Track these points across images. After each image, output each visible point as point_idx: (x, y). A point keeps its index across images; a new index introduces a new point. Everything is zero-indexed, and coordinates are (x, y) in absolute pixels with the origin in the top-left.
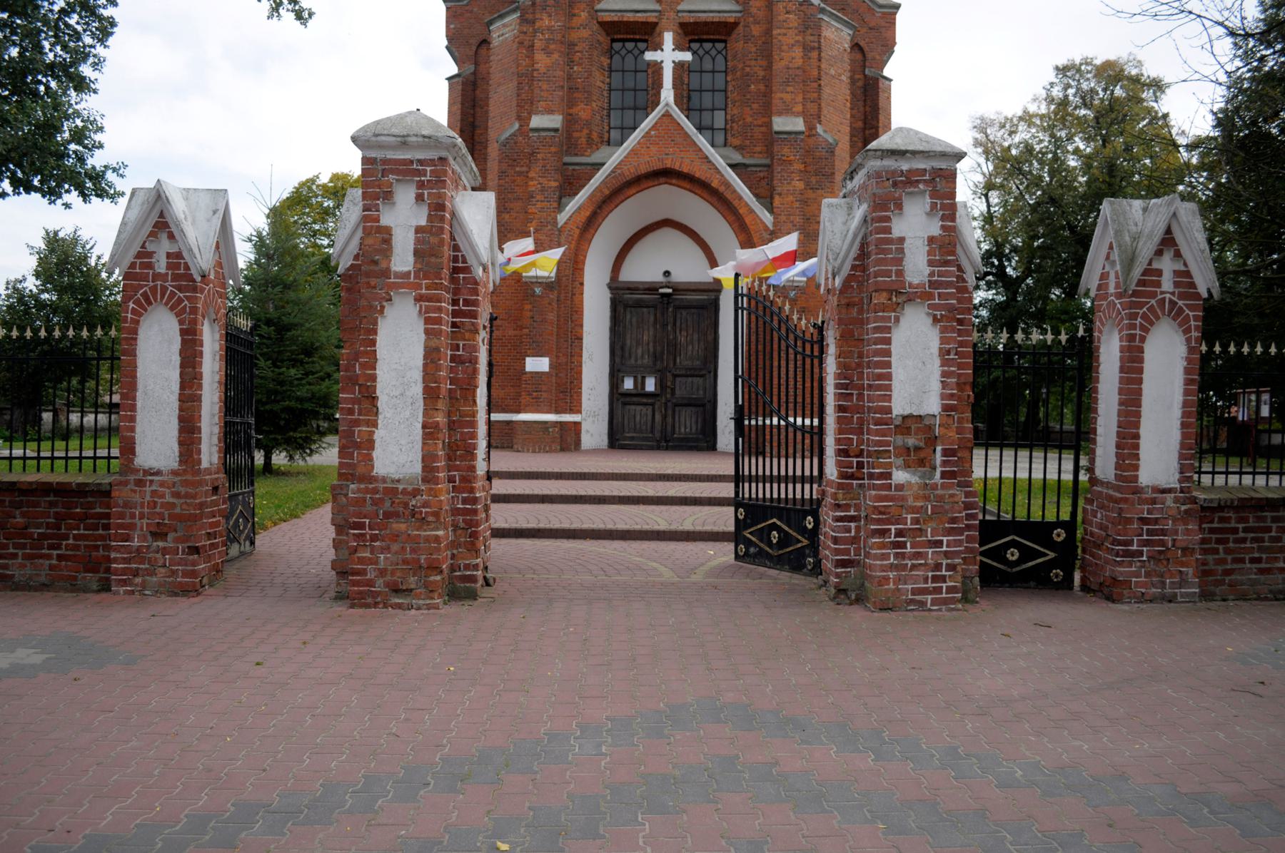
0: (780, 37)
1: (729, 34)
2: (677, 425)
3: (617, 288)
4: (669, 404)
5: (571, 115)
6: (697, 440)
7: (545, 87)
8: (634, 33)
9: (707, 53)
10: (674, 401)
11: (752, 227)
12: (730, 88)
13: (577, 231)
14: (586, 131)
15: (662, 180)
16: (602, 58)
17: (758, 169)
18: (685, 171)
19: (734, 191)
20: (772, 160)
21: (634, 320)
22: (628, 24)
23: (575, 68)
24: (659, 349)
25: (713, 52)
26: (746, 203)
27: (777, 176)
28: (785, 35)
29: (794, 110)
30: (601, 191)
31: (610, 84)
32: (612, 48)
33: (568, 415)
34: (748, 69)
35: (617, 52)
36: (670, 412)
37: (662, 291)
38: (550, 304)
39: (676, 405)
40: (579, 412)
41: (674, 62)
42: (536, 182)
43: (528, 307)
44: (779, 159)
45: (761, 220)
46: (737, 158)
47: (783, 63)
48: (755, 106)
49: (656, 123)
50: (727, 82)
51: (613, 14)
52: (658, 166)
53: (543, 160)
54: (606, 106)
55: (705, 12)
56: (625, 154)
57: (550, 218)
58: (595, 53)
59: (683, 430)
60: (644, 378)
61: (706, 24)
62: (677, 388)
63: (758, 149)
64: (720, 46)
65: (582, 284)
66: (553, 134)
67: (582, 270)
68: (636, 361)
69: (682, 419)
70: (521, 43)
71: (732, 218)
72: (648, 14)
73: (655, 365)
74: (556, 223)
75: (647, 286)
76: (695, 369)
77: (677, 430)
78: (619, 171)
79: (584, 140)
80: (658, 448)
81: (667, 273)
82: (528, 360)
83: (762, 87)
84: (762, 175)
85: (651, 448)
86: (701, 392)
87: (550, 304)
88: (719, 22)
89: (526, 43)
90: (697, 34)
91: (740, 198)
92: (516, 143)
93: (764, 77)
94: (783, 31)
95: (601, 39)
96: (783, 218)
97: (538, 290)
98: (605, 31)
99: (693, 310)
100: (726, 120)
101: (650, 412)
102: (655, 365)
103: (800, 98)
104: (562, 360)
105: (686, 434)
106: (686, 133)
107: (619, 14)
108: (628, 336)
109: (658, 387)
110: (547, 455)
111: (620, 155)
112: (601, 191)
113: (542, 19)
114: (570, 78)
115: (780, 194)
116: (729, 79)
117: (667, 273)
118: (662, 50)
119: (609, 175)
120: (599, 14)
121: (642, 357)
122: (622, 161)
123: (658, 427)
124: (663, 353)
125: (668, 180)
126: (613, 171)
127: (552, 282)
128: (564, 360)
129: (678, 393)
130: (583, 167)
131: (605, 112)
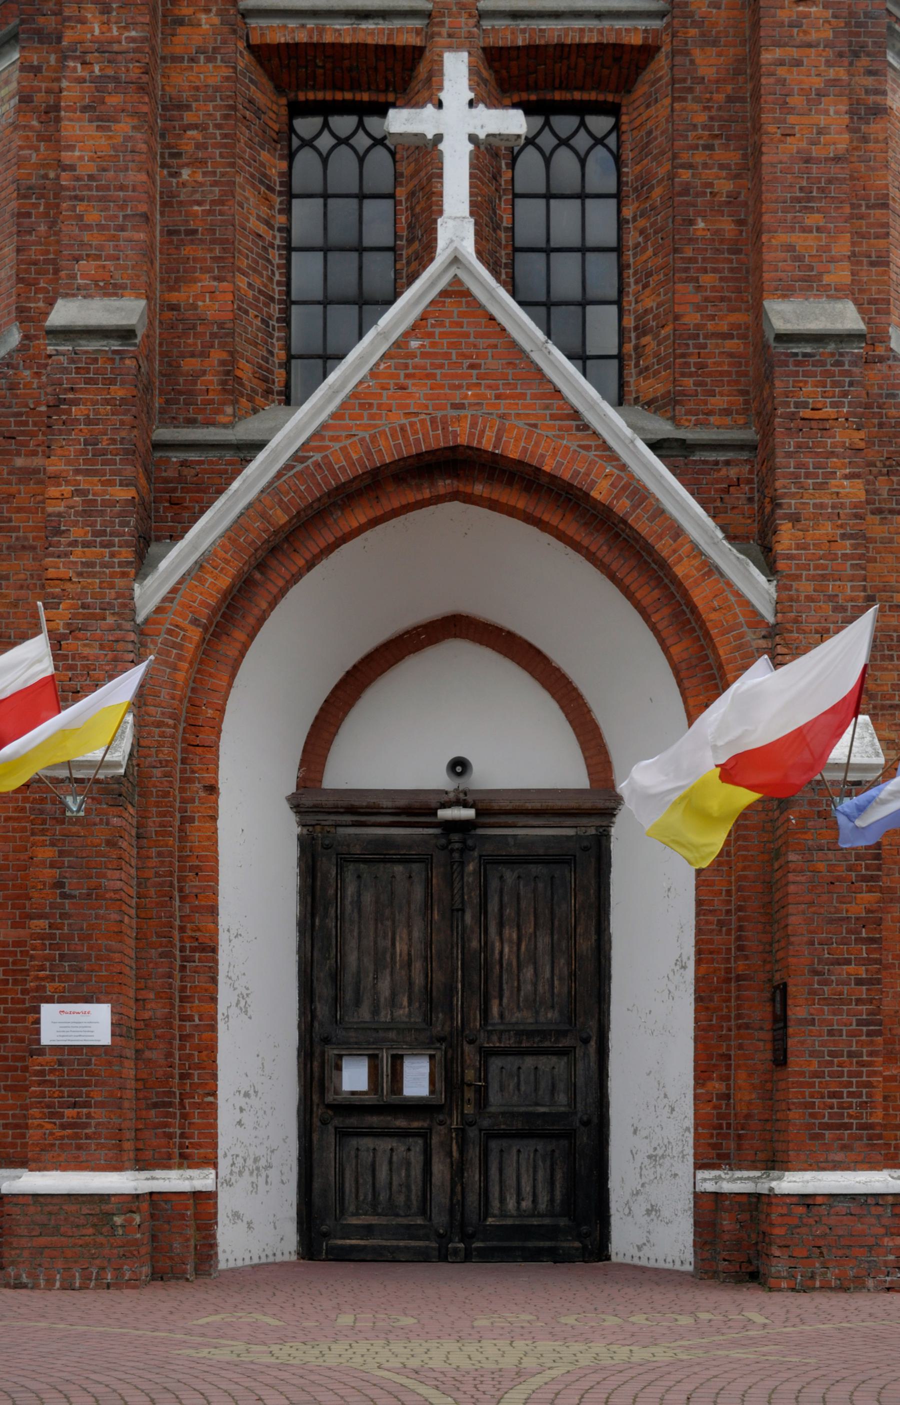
0: (781, 71)
1: (627, 85)
2: (495, 1191)
3: (317, 809)
4: (473, 1133)
5: (173, 308)
6: (552, 1232)
7: (93, 216)
8: (355, 86)
9: (564, 142)
10: (486, 1123)
11: (710, 617)
12: (632, 238)
13: (195, 634)
14: (217, 355)
15: (444, 485)
16: (264, 156)
17: (722, 457)
18: (513, 453)
19: (660, 512)
20: (767, 429)
21: (368, 898)
22: (336, 51)
23: (186, 174)
24: (439, 977)
25: (582, 141)
26: (695, 546)
27: (785, 465)
28: (798, 63)
29: (826, 279)
30: (263, 515)
31: (288, 230)
32: (292, 130)
33: (174, 1174)
34: (685, 175)
35: (307, 143)
36: (473, 1153)
37: (445, 814)
38: (110, 843)
39: (490, 1135)
40: (211, 1162)
41: (473, 138)
42: (67, 489)
43: (46, 853)
44: (792, 417)
45: (738, 594)
46: (664, 428)
47: (792, 145)
48: (708, 280)
49: (423, 318)
50: (621, 223)
51: (292, 24)
52: (434, 440)
53: (89, 422)
54: (277, 291)
55: (556, 15)
56: (332, 407)
57: (110, 594)
58: (244, 135)
59: (511, 1204)
60: (397, 1062)
61: (562, 50)
62: (494, 1086)
63: (719, 402)
64: (600, 124)
65: (212, 789)
66: (116, 346)
67: (213, 748)
68: (375, 1011)
69: (510, 1173)
70: (25, 99)
71: (649, 595)
72: (397, 23)
73: (429, 1021)
74: (128, 607)
75: (402, 802)
76: (544, 1034)
77: (495, 1203)
78: (318, 457)
79: (212, 379)
80: (443, 1256)
81: (459, 767)
82: (49, 1012)
83: (727, 226)
84: (733, 472)
85: (422, 1257)
86: (562, 1098)
87: (110, 843)
88: (599, 46)
89: (39, 98)
90: (536, 88)
91: (677, 532)
92: (12, 387)
93: (734, 196)
94: (795, 53)
95: (261, 99)
96: (805, 587)
97: (73, 803)
98: (272, 77)
99: (535, 869)
100: (622, 331)
101: (416, 1158)
102: (429, 1021)
103: (842, 246)
104: (156, 1010)
105: (520, 1214)
106: (514, 344)
107: (311, 24)
108: (352, 943)
109: (440, 1085)
110: (107, 1296)
111: (318, 410)
112: (263, 515)
113: (83, 21)
114: (169, 201)
115: (795, 519)
116: (628, 213)
117: (459, 767)
118: (440, 105)
119: (287, 467)
120: (253, 23)
121: (393, 1002)
122: (324, 426)
123: (440, 1197)
124: (450, 990)
125: (462, 487)
126: (297, 458)
127: (117, 779)
128: (162, 1012)
129: (495, 1098)
130: (213, 455)
131: (275, 310)
